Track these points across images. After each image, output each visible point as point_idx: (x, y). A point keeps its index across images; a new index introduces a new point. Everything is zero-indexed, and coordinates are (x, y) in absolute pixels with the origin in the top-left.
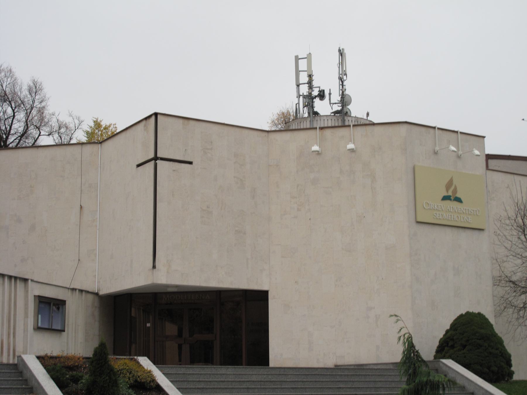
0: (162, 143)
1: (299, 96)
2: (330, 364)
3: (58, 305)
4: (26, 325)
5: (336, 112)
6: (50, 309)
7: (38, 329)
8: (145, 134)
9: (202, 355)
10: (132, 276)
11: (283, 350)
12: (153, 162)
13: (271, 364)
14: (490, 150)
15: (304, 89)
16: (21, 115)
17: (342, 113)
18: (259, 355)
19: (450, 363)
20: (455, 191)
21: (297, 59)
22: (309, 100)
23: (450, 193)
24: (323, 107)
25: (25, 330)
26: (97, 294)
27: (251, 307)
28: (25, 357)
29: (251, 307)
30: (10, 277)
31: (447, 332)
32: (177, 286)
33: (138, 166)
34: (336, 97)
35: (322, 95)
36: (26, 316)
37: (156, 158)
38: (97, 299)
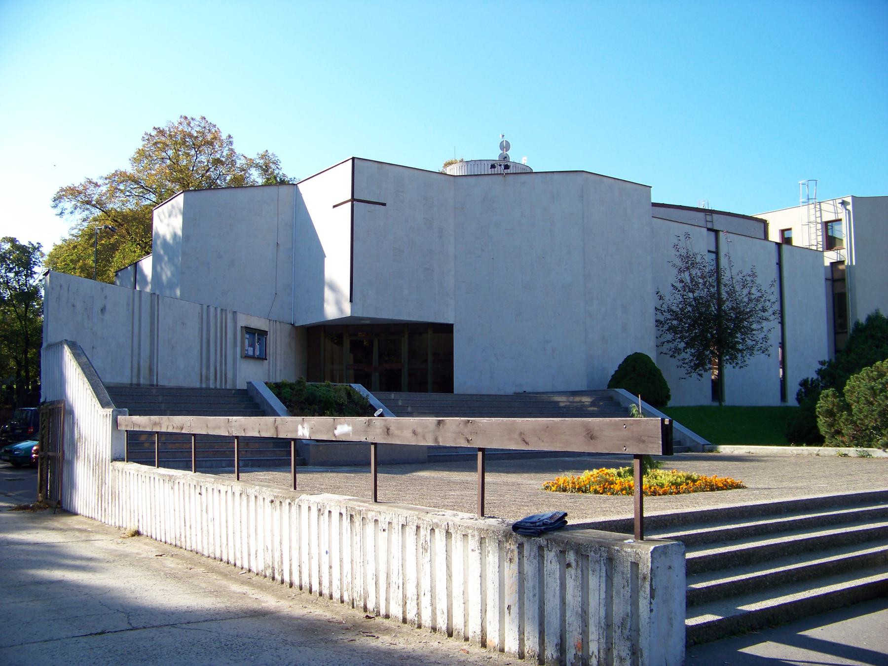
2: (510, 391)
4: (235, 353)
14: (653, 200)
26: (293, 325)
32: (370, 319)
33: (334, 207)
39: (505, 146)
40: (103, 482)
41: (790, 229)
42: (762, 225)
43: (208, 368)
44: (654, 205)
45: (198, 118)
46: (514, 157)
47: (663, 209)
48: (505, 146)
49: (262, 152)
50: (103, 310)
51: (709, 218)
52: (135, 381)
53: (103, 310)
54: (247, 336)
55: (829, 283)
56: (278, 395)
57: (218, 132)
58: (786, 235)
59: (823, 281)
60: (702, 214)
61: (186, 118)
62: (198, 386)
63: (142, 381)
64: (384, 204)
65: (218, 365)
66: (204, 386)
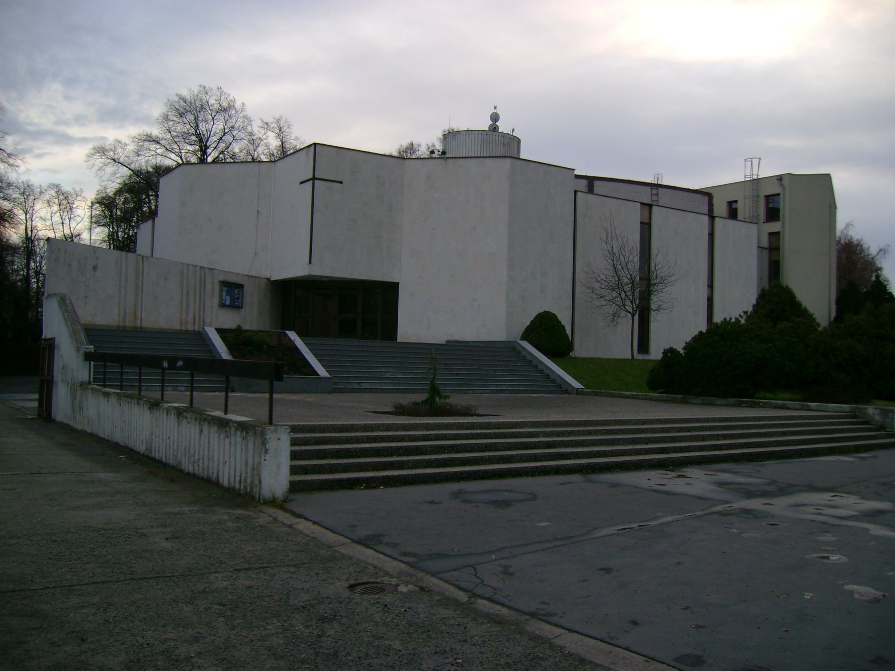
0: (327, 169)
2: (441, 339)
3: (240, 287)
6: (233, 292)
7: (222, 305)
9: (346, 330)
10: (294, 266)
11: (415, 324)
12: (310, 183)
19: (525, 344)
26: (269, 279)
27: (384, 296)
28: (207, 329)
29: (384, 296)
31: (754, 306)
33: (301, 183)
37: (314, 179)
39: (495, 118)
40: (75, 397)
41: (736, 201)
42: (706, 198)
44: (577, 177)
45: (215, 88)
46: (504, 127)
47: (612, 183)
48: (495, 118)
49: (277, 117)
50: (95, 268)
51: (654, 192)
52: (121, 324)
53: (95, 268)
54: (225, 288)
55: (766, 253)
56: (224, 339)
57: (234, 101)
58: (734, 206)
59: (755, 250)
60: (648, 189)
61: (205, 87)
62: (178, 328)
64: (341, 183)
65: (197, 312)
66: (183, 328)
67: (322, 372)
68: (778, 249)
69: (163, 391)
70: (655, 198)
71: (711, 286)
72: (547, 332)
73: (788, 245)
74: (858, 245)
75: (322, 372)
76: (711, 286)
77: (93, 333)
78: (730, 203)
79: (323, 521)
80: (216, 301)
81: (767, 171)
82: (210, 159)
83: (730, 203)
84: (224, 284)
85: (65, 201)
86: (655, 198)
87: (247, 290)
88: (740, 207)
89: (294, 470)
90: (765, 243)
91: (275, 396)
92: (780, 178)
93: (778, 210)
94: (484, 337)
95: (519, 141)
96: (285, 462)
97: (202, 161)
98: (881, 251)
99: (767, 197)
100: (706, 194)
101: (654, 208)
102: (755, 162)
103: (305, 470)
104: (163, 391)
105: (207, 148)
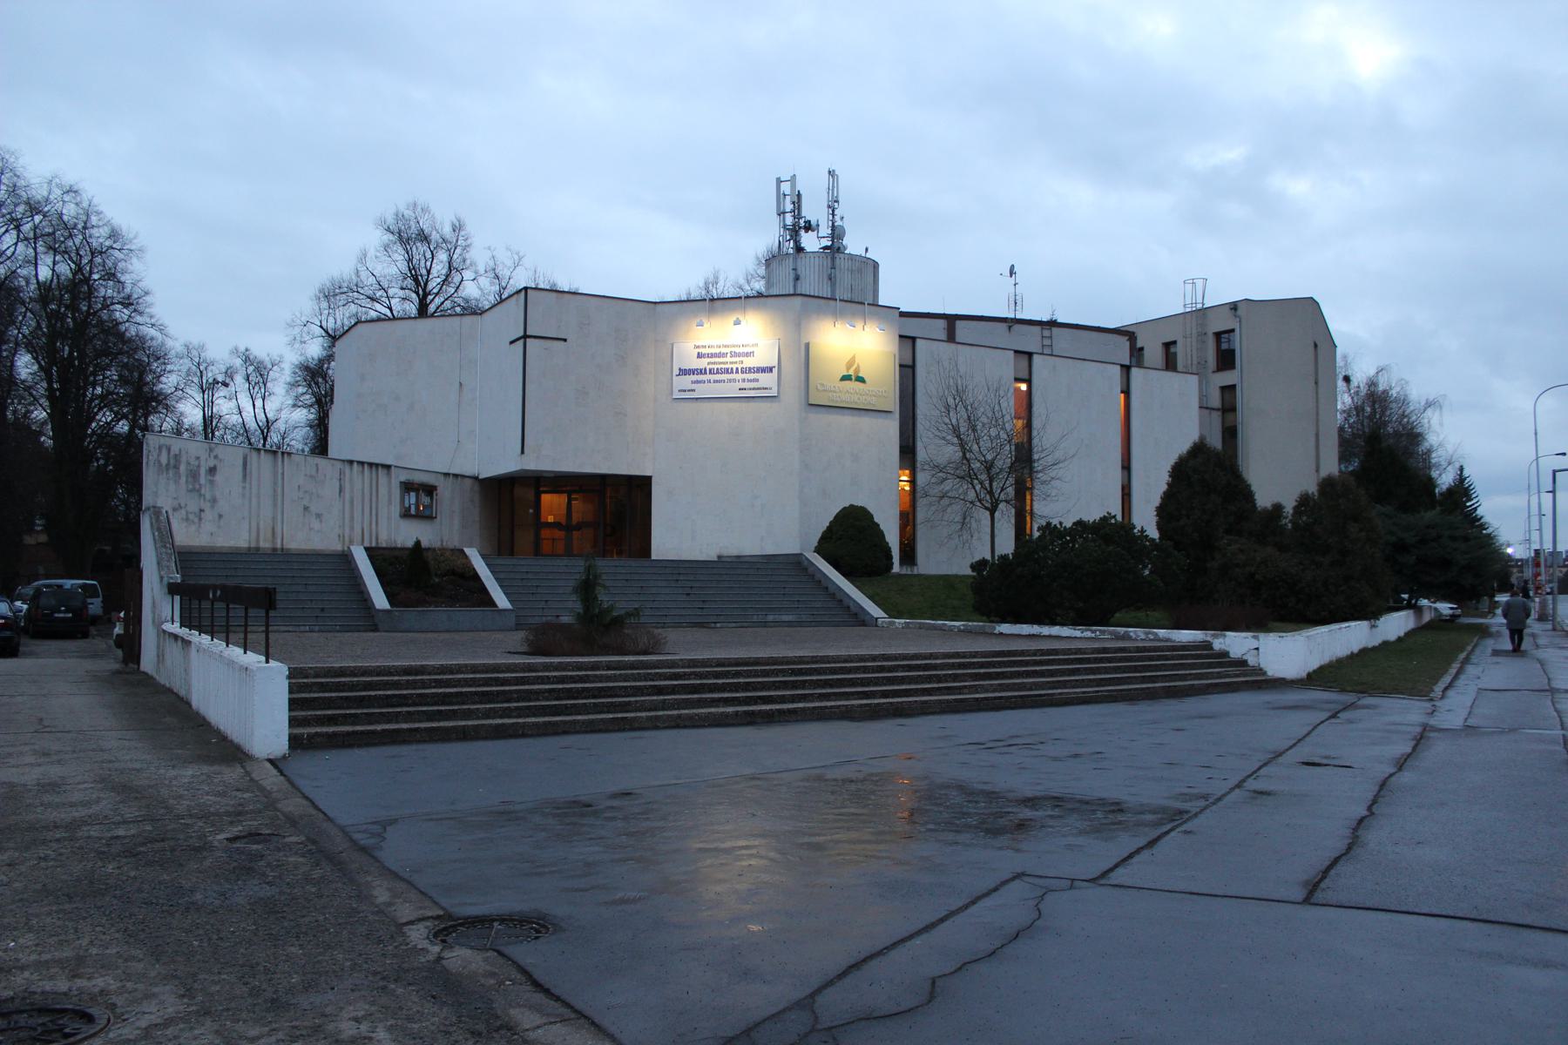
1: (785, 226)
3: (430, 490)
5: (825, 248)
7: (406, 514)
8: (514, 308)
10: (505, 463)
11: (677, 533)
12: (521, 343)
13: (656, 554)
15: (789, 220)
16: (442, 256)
17: (834, 249)
18: (645, 550)
20: (857, 370)
21: (779, 181)
22: (794, 232)
23: (851, 372)
24: (810, 242)
25: (389, 518)
26: (476, 478)
30: (371, 465)
34: (825, 230)
35: (808, 227)
36: (390, 498)
37: (525, 337)
38: (477, 488)
41: (1174, 343)
42: (1124, 343)
43: (352, 528)
51: (1046, 333)
52: (253, 545)
60: (1037, 329)
63: (262, 544)
67: (502, 601)
68: (1233, 409)
69: (267, 632)
70: (1047, 342)
71: (1127, 467)
72: (851, 539)
73: (1248, 401)
74: (1396, 400)
75: (502, 601)
76: (1127, 467)
77: (187, 558)
78: (1168, 346)
79: (348, 786)
80: (396, 510)
81: (1219, 295)
82: (432, 308)
83: (1168, 346)
84: (408, 487)
85: (258, 373)
86: (1047, 342)
87: (445, 490)
88: (1179, 349)
89: (293, 722)
90: (1215, 400)
91: (250, 636)
92: (1234, 307)
93: (1232, 352)
94: (771, 549)
95: (876, 265)
96: (282, 715)
97: (423, 311)
98: (1429, 404)
99: (1218, 335)
100: (1128, 333)
101: (1035, 357)
102: (1199, 284)
103: (304, 722)
104: (267, 632)
105: (426, 295)
